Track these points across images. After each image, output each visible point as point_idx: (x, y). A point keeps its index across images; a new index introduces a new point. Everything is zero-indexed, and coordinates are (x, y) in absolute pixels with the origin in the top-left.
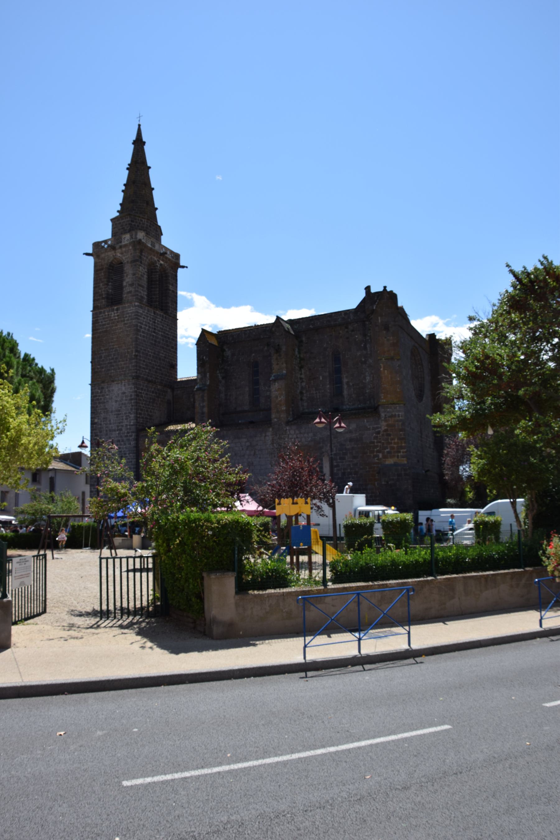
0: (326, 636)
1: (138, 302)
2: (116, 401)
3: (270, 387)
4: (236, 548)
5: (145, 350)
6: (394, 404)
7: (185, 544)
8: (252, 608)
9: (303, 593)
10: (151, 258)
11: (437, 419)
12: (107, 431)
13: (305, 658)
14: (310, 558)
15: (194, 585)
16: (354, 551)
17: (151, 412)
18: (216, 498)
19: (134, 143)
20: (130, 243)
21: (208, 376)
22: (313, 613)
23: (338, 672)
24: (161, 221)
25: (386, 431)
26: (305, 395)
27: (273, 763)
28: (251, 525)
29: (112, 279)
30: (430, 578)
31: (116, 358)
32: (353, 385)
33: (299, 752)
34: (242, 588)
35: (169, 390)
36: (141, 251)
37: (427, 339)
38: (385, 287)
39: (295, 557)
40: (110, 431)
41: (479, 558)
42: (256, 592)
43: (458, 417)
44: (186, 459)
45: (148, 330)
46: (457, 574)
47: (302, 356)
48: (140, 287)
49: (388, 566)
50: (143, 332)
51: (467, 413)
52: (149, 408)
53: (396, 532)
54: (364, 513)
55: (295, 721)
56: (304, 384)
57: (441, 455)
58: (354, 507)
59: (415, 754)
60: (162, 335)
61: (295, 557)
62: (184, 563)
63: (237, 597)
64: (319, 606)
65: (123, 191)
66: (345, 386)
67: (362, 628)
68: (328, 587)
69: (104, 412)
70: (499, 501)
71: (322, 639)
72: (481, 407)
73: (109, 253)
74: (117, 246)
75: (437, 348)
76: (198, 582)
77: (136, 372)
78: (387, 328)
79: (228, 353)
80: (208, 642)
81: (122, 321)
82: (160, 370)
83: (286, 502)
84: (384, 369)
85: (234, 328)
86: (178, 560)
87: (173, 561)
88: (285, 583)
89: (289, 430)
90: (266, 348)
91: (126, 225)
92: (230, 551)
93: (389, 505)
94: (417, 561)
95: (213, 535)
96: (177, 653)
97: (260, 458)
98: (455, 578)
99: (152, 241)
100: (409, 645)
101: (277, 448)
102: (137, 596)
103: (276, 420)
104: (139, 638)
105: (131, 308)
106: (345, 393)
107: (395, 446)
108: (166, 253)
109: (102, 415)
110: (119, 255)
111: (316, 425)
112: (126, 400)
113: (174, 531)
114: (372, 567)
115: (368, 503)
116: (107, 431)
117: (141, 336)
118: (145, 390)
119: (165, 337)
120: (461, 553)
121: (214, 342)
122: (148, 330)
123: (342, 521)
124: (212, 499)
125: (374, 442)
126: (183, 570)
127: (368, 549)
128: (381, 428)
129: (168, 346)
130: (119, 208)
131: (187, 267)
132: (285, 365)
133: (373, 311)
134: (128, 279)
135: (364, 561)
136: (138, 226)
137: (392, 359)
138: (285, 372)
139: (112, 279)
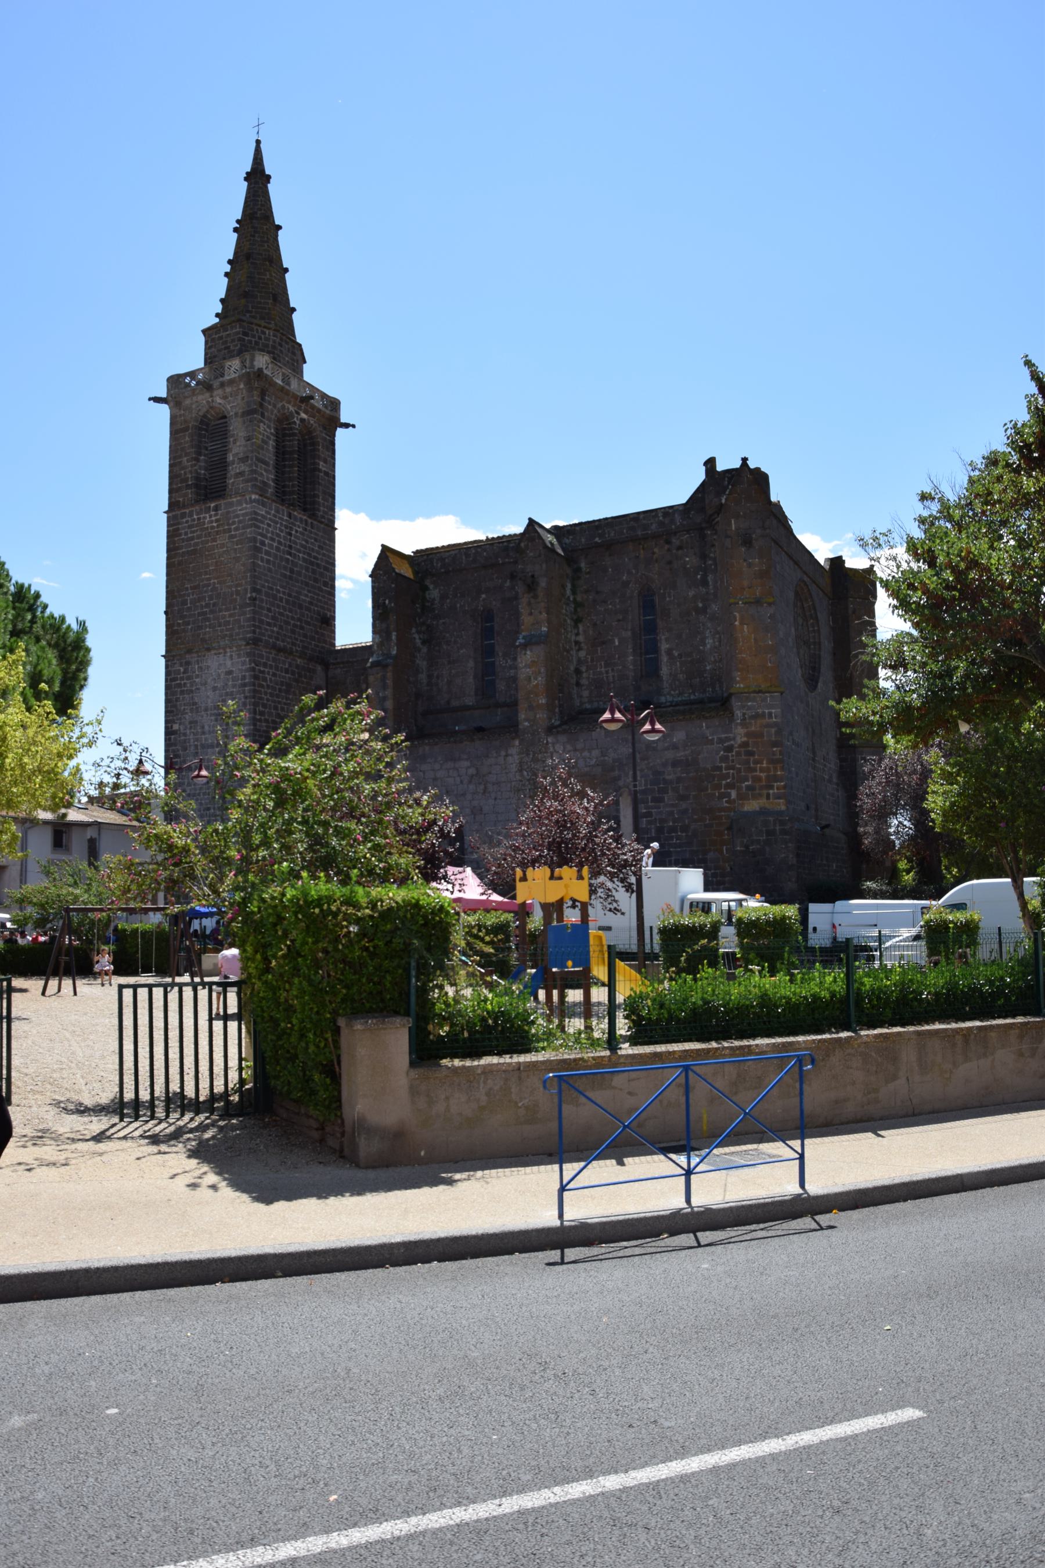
0: (614, 1162)
1: (256, 493)
2: (215, 689)
3: (515, 659)
4: (413, 964)
5: (272, 589)
6: (760, 692)
7: (299, 955)
8: (447, 1098)
9: (565, 1064)
10: (283, 407)
11: (852, 708)
12: (196, 746)
13: (561, 1216)
14: (587, 995)
15: (318, 1047)
16: (678, 973)
17: (283, 709)
18: (372, 856)
19: (248, 177)
20: (241, 377)
21: (394, 637)
22: (580, 1113)
23: (637, 1251)
24: (303, 333)
25: (745, 745)
26: (585, 675)
27: (449, 1528)
28: (448, 913)
29: (206, 448)
30: (844, 1034)
31: (214, 605)
32: (680, 656)
33: (522, 1490)
34: (425, 1052)
35: (319, 668)
36: (263, 393)
37: (827, 567)
38: (745, 460)
39: (555, 992)
40: (203, 746)
41: (948, 991)
42: (457, 1062)
43: (896, 705)
44: (306, 774)
45: (278, 549)
46: (903, 1025)
47: (579, 599)
48: (260, 464)
49: (753, 1006)
50: (267, 553)
51: (915, 696)
52: (279, 702)
53: (767, 944)
54: (701, 905)
55: (522, 1388)
56: (582, 654)
57: (852, 795)
58: (680, 894)
59: (836, 1503)
60: (304, 560)
61: (555, 992)
62: (297, 997)
63: (414, 1073)
64: (596, 1095)
65: (227, 275)
66: (665, 659)
67: (693, 1144)
68: (620, 1052)
69: (192, 710)
70: (975, 882)
71: (603, 1170)
72: (944, 684)
73: (200, 397)
74: (216, 384)
75: (846, 590)
76: (326, 1039)
77: (254, 632)
78: (747, 542)
79: (434, 593)
80: (347, 1173)
81: (225, 531)
82: (302, 628)
83: (539, 874)
84: (742, 623)
85: (446, 544)
86: (285, 990)
87: (275, 994)
88: (521, 1042)
89: (553, 744)
90: (508, 584)
91: (233, 341)
92: (400, 971)
93: (749, 892)
94: (816, 997)
95: (362, 934)
96: (268, 1201)
97: (495, 799)
98: (899, 1033)
99: (283, 374)
100: (802, 1184)
101: (529, 780)
102: (216, 1070)
103: (526, 724)
104: (194, 1162)
105: (243, 505)
106: (665, 671)
107: (763, 775)
108: (312, 398)
109: (187, 717)
110: (219, 400)
111: (605, 725)
112: (234, 686)
113: (275, 925)
114: (717, 1008)
115: (707, 889)
116: (196, 746)
117: (262, 560)
118: (271, 667)
119: (312, 563)
120: (911, 981)
121: (407, 571)
122: (278, 549)
123: (654, 919)
124: (365, 857)
125: (720, 768)
126: (295, 1012)
127: (710, 970)
128: (734, 739)
129: (316, 580)
130: (219, 308)
131: (354, 426)
132: (545, 615)
133: (720, 508)
134: (237, 449)
135: (700, 995)
136: (256, 343)
137: (758, 602)
138: (545, 629)
139: (206, 448)
